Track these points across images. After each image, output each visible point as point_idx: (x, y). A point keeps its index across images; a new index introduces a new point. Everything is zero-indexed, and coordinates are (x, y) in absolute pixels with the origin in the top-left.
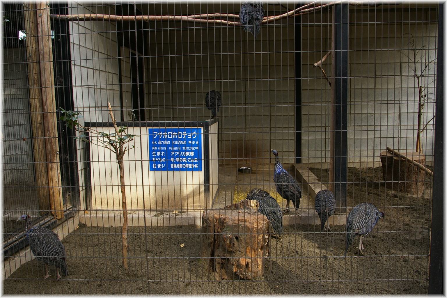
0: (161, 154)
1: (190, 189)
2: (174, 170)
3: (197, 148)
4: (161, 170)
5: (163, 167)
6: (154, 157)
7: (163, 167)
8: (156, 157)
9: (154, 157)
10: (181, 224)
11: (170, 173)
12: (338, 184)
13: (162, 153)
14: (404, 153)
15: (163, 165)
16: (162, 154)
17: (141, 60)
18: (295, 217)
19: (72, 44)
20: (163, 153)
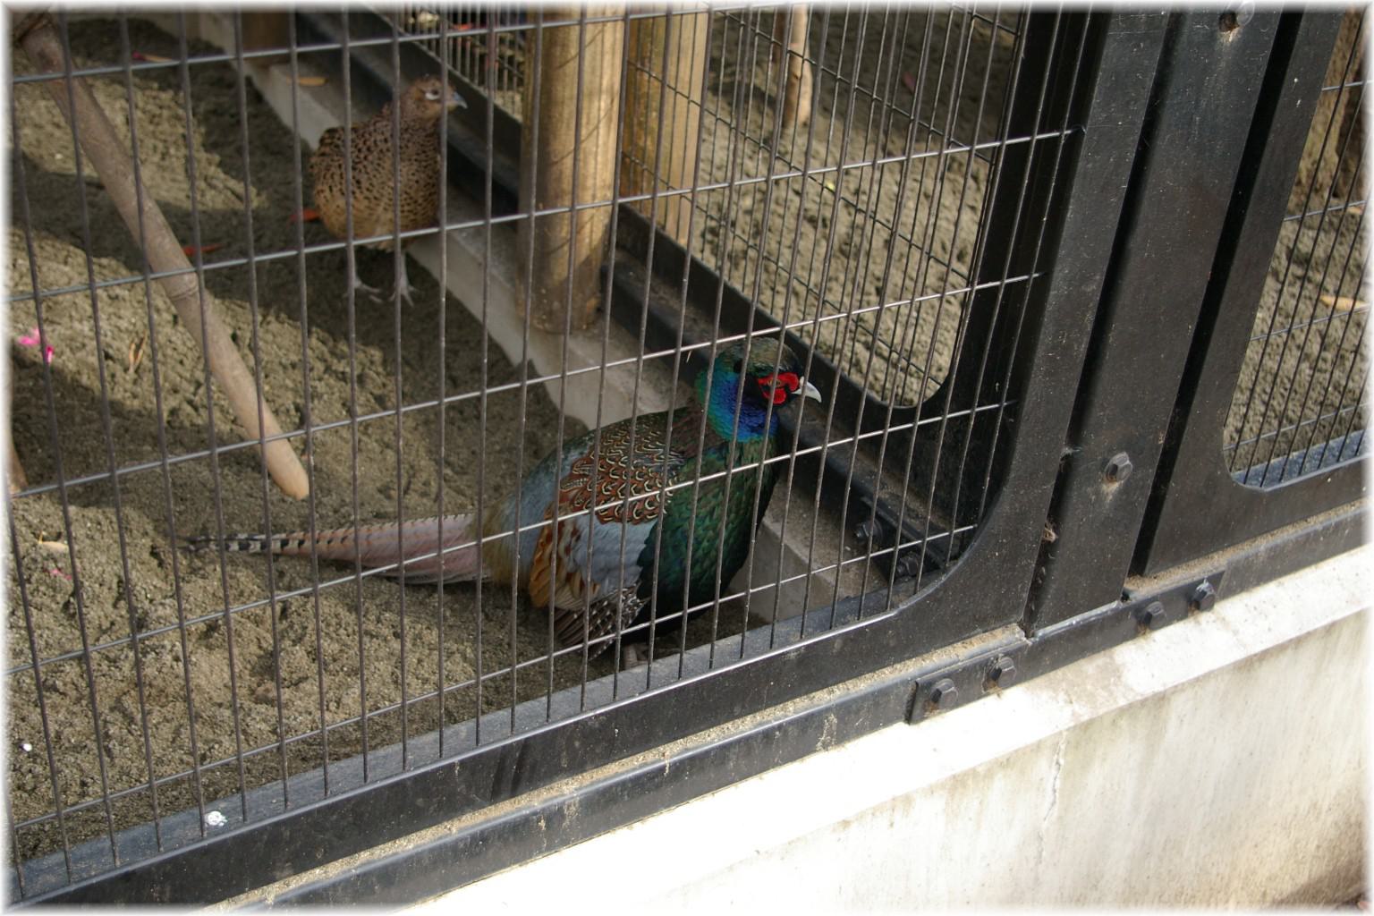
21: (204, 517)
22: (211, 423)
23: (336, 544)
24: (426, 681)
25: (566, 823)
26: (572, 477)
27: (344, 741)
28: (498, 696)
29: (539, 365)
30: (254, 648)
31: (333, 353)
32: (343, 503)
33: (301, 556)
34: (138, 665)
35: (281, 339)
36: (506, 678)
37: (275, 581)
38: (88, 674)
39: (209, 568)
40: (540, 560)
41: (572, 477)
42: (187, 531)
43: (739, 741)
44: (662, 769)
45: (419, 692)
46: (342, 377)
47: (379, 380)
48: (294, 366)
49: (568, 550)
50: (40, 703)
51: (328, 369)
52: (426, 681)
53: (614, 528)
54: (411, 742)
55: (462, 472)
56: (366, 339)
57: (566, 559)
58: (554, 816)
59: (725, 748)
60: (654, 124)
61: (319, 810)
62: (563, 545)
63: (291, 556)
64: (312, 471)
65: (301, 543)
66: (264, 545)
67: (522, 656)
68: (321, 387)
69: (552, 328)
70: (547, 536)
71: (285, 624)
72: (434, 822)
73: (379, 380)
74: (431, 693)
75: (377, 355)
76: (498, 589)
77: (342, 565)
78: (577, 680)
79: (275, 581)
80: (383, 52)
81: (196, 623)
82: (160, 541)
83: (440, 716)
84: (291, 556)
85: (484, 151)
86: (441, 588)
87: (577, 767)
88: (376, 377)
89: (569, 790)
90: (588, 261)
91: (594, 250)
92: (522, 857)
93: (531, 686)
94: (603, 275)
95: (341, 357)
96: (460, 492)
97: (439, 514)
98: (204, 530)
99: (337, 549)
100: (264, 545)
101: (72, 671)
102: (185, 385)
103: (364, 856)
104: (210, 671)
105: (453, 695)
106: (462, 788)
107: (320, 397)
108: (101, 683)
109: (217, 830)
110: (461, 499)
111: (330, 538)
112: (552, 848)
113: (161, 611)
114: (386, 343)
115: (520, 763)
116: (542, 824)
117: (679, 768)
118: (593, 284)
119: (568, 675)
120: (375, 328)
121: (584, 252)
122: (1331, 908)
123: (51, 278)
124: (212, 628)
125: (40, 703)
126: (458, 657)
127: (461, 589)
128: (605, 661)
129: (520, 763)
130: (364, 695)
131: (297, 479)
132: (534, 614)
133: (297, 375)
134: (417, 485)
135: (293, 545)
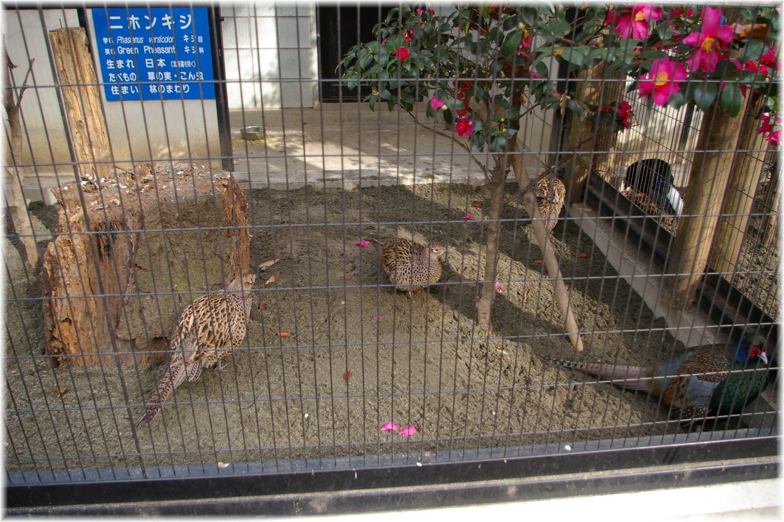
0: (125, 64)
1: (159, 156)
2: (155, 97)
3: (105, 40)
4: (130, 97)
5: (133, 92)
6: (112, 71)
7: (133, 92)
8: (116, 71)
9: (112, 71)
10: (303, 180)
11: (152, 107)
12: (596, 295)
13: (128, 61)
14: (283, 184)
15: (134, 89)
16: (128, 65)
17: (646, 168)
18: (432, 185)
19: (547, 121)
20: (130, 63)
21: (549, 351)
22: (551, 320)
23: (594, 369)
24: (624, 421)
25: (684, 479)
26: (688, 361)
27: (594, 435)
28: (648, 432)
29: (669, 321)
30: (565, 398)
31: (592, 304)
32: (595, 356)
33: (580, 371)
34: (528, 394)
35: (577, 295)
36: (652, 426)
37: (572, 378)
38: (512, 394)
39: (550, 369)
40: (671, 388)
41: (688, 361)
42: (543, 355)
43: (750, 466)
44: (721, 469)
45: (621, 425)
46: (595, 312)
47: (608, 315)
48: (578, 306)
49: (683, 386)
50: (497, 401)
51: (590, 309)
52: (624, 421)
53: (706, 383)
54: (548, 444)
55: (636, 352)
56: (604, 301)
57: (682, 389)
58: (681, 475)
59: (746, 467)
60: (726, 241)
61: (608, 453)
62: (681, 385)
63: (577, 370)
64: (585, 342)
65: (582, 366)
66: (569, 364)
67: (658, 420)
68: (588, 315)
69: (676, 306)
70: (674, 381)
71: (575, 392)
72: (642, 466)
73: (608, 315)
74: (625, 426)
75: (607, 307)
76: (655, 398)
77: (594, 376)
78: (675, 433)
79: (572, 378)
80: (639, 221)
81: (546, 386)
82: (534, 356)
83: (629, 433)
84: (577, 370)
85: (653, 241)
86: (636, 393)
87: (693, 460)
88: (607, 314)
89: (687, 468)
90: (693, 286)
91: (696, 282)
92: (667, 487)
93: (660, 431)
94: (698, 291)
95: (595, 306)
96: (635, 359)
97: (629, 365)
98: (549, 356)
99: (594, 371)
100: (569, 364)
101: (507, 393)
102: (542, 307)
103: (616, 471)
104: (548, 400)
105: (633, 428)
106: (653, 457)
107: (587, 318)
108: (517, 398)
109: (567, 451)
110: (636, 362)
111: (592, 367)
112: (677, 486)
113: (535, 379)
114: (609, 303)
115: (675, 453)
116: (676, 477)
117: (728, 470)
118: (694, 294)
119: (672, 430)
120: (607, 299)
121: (692, 282)
122: (532, 6)
123: (501, 265)
124: (551, 388)
125: (497, 401)
126: (635, 415)
127: (643, 393)
128: (686, 428)
129: (675, 453)
130: (603, 421)
131: (581, 347)
132: (665, 407)
133: (579, 309)
134: (620, 354)
135: (579, 366)
